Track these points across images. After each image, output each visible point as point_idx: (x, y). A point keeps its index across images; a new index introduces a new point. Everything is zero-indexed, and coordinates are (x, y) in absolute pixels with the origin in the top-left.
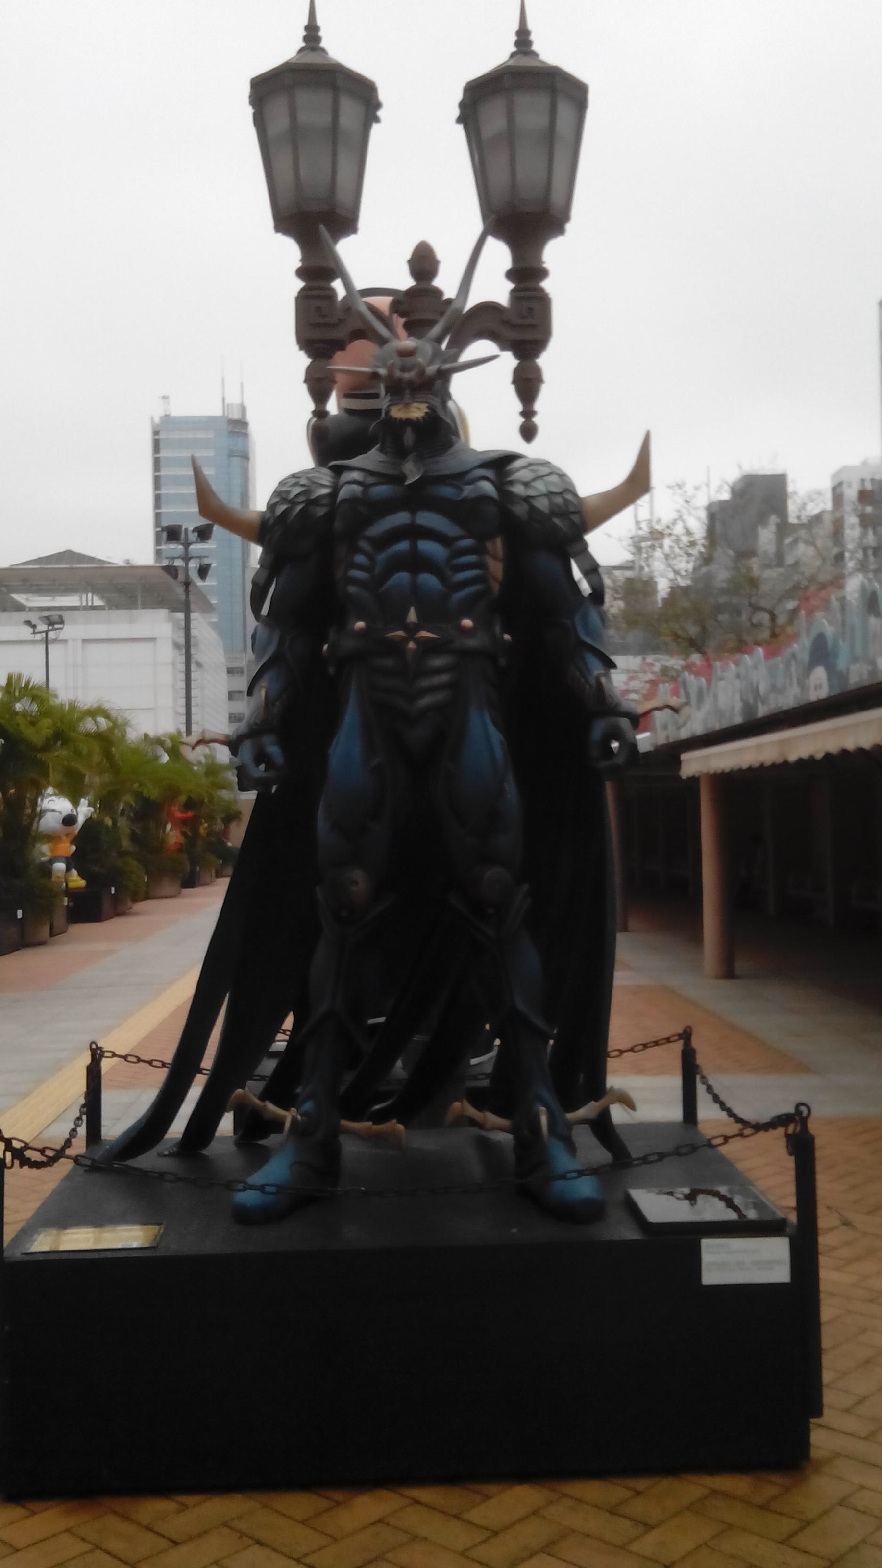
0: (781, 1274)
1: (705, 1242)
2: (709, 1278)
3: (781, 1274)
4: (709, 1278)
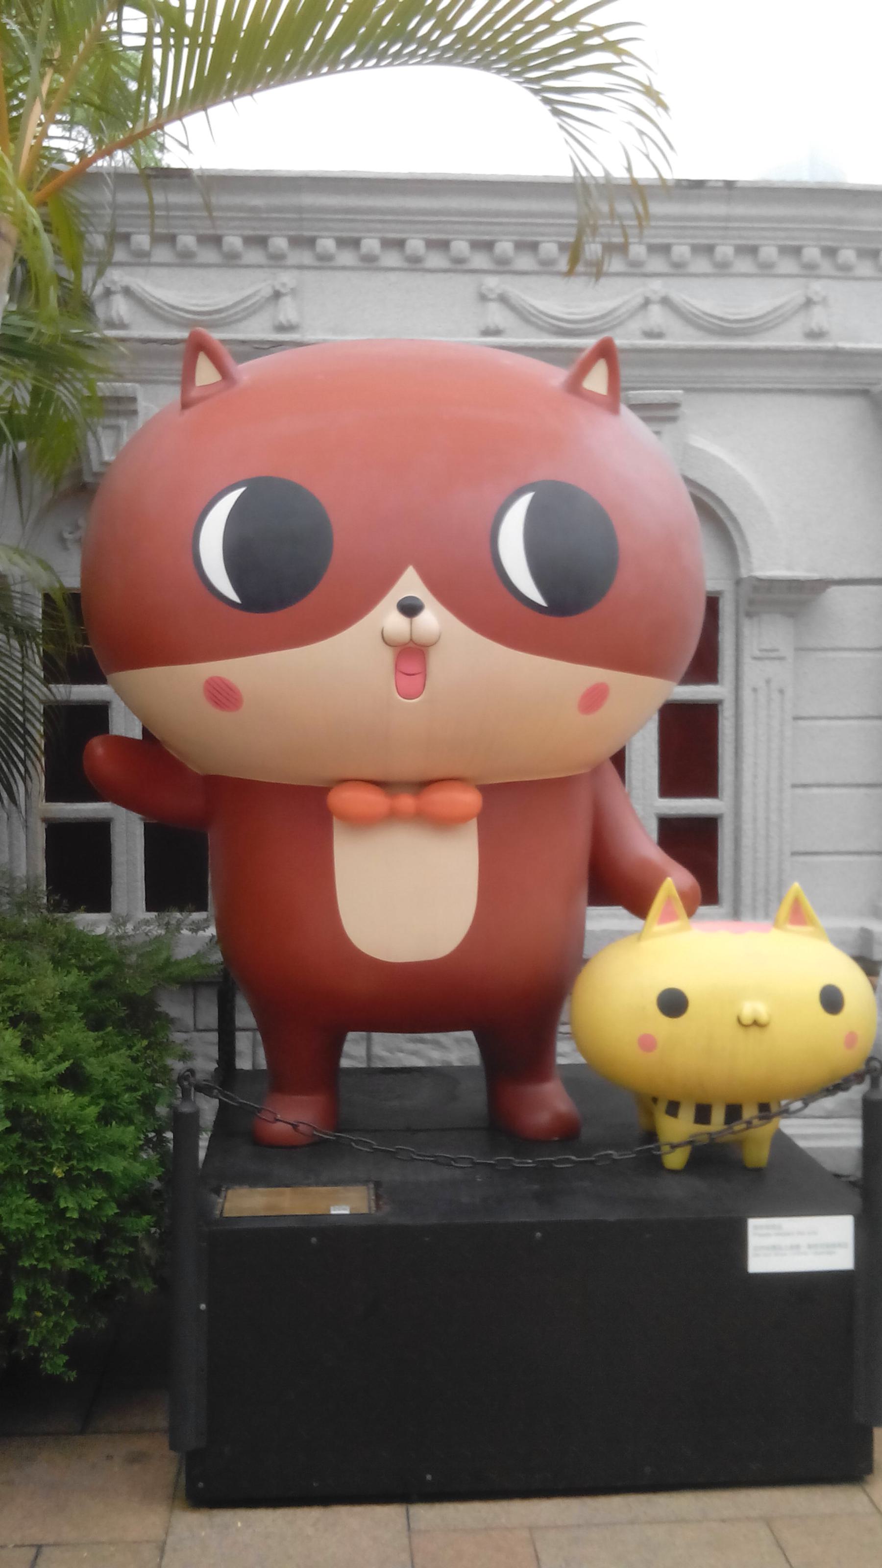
0: (842, 1259)
1: (753, 1224)
2: (759, 1262)
3: (842, 1259)
4: (759, 1262)
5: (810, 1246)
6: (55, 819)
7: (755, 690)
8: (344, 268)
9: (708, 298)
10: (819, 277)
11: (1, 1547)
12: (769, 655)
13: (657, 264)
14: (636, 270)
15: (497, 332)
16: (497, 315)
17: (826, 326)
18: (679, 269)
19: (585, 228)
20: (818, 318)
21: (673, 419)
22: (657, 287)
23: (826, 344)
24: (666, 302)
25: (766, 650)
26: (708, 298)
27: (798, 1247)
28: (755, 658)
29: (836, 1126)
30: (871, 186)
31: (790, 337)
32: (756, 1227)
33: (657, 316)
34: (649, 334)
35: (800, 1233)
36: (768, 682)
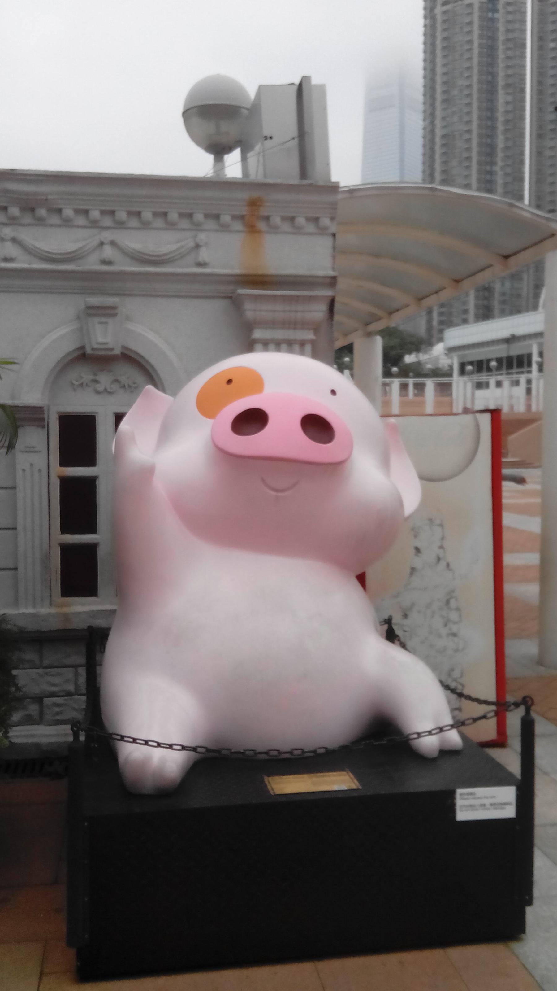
0: (510, 812)
1: (459, 791)
2: (462, 816)
3: (510, 812)
4: (462, 816)
5: (491, 805)
6: (64, 542)
7: (24, 470)
8: (52, 226)
9: (136, 241)
10: (202, 231)
11: (324, 988)
12: (30, 450)
13: (107, 221)
14: (94, 224)
15: (108, 263)
16: (11, 250)
17: (207, 260)
18: (120, 225)
19: (254, 204)
20: (204, 255)
21: (115, 315)
22: (107, 236)
23: (207, 270)
24: (113, 243)
25: (28, 447)
26: (136, 241)
27: (484, 805)
28: (21, 451)
29: (33, 736)
30: (184, 177)
31: (91, 264)
32: (461, 794)
33: (108, 252)
34: (105, 262)
35: (486, 797)
36: (32, 465)
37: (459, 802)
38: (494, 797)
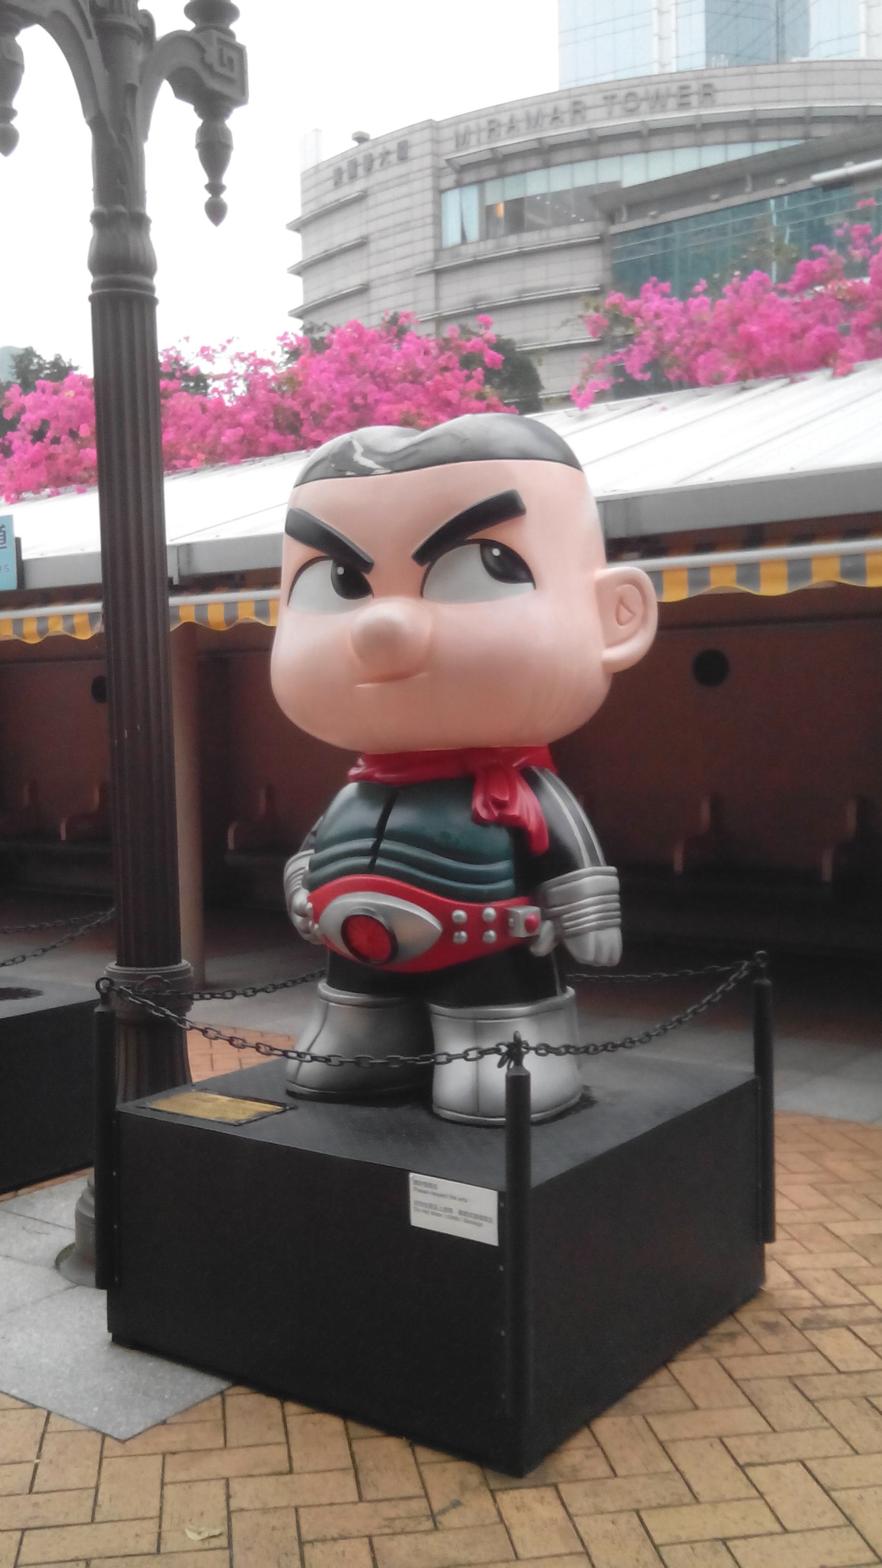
2: (419, 1219)
5: (461, 1213)
27: (450, 1210)
32: (416, 1182)
37: (414, 1196)
38: (464, 1200)
